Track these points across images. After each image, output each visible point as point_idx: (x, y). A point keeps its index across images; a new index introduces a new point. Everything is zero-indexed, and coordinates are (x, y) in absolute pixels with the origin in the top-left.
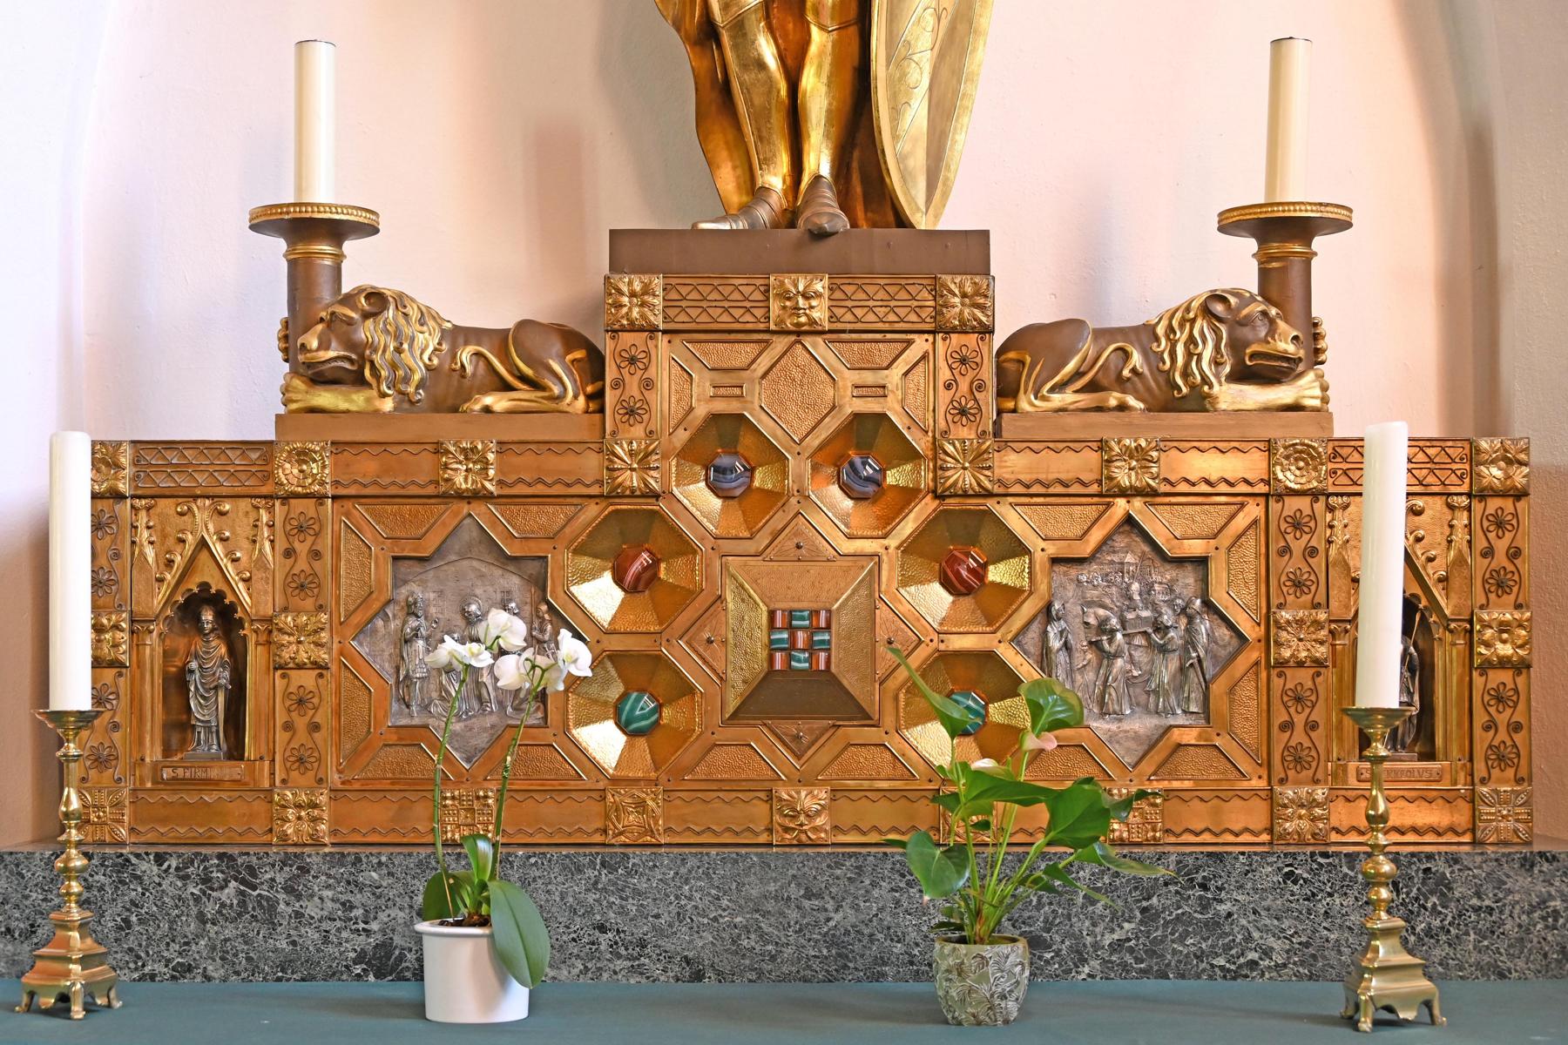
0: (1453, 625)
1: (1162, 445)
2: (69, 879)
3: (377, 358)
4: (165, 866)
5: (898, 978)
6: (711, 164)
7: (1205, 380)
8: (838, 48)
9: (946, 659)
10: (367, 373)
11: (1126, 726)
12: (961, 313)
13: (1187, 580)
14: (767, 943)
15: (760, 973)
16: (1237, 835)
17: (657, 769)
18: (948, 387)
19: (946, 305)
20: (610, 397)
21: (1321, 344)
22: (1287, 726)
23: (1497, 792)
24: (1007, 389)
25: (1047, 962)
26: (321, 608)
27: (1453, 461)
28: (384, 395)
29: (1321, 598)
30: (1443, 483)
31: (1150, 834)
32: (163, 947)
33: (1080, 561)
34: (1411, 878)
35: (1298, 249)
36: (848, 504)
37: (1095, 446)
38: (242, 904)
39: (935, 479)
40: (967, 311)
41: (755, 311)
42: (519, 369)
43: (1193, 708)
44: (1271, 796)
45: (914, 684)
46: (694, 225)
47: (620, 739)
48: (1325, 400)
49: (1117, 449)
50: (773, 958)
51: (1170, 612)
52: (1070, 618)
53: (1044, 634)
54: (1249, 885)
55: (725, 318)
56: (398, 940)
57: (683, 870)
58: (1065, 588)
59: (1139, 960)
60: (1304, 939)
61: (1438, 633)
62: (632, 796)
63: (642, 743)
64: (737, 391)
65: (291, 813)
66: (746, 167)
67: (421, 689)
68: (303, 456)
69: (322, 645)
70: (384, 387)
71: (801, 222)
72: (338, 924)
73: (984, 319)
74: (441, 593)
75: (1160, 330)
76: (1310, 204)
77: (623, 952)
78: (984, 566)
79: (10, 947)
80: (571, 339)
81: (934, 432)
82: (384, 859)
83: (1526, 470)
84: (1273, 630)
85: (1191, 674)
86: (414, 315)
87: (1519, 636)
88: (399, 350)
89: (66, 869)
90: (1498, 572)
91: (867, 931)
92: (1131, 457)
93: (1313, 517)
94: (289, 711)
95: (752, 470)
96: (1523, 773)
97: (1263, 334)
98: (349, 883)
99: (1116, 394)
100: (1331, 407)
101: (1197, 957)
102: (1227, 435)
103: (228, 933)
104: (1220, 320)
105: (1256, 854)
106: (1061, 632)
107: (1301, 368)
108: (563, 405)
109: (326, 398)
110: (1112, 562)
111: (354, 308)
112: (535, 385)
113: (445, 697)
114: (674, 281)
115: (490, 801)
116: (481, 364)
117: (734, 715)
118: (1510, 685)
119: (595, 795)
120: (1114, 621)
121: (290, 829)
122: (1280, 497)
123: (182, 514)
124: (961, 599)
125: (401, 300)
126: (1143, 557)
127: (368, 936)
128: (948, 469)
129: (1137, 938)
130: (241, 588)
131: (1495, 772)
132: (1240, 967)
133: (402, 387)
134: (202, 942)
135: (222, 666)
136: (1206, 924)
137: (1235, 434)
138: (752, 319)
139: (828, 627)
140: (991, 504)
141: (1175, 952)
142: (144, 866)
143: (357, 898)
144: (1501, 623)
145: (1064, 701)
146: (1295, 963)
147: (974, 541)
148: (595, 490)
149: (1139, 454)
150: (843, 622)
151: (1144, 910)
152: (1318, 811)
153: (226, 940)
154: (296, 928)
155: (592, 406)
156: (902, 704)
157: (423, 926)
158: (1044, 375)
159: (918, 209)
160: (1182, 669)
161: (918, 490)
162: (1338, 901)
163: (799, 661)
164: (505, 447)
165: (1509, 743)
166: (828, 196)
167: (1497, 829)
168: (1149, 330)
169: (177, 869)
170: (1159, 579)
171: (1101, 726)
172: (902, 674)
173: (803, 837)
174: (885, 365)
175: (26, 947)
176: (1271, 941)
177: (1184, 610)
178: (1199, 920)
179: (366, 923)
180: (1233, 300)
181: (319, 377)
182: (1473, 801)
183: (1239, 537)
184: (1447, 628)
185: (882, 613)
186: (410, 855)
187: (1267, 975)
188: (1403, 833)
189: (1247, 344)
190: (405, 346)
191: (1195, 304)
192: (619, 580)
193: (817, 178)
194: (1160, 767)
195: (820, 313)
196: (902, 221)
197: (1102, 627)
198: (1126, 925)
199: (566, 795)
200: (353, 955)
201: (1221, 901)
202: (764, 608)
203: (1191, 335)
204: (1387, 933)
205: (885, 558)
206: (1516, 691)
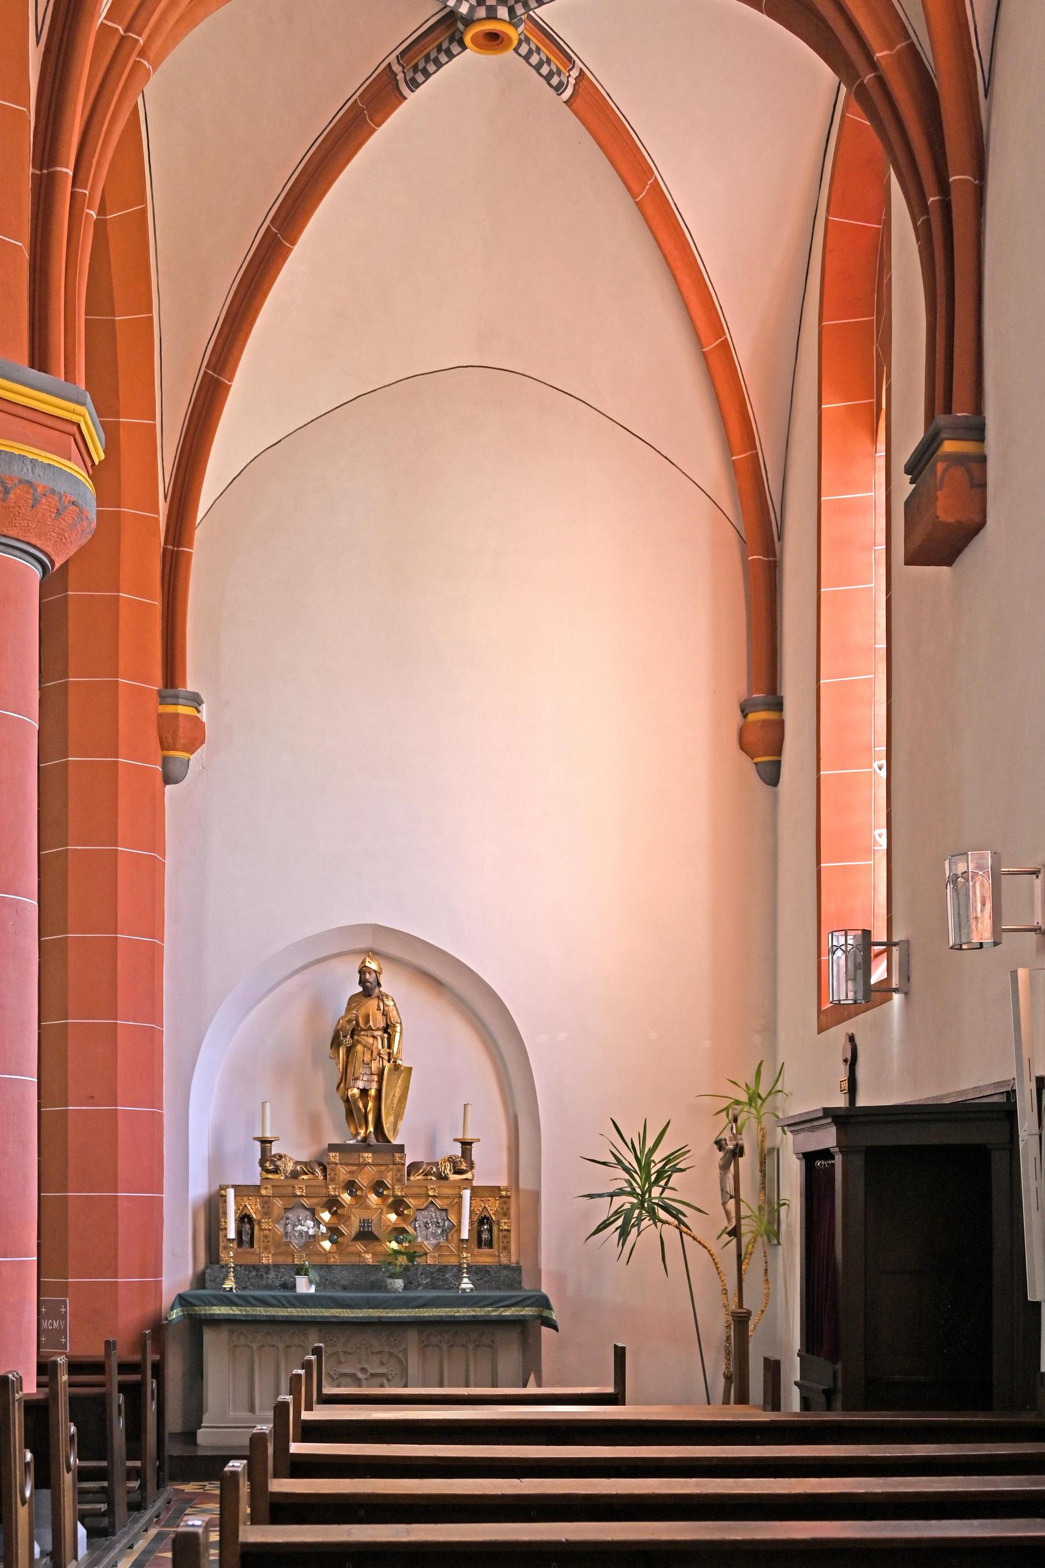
3: (281, 1168)
8: (374, 1106)
11: (431, 1242)
13: (444, 1213)
20: (328, 1177)
28: (282, 1176)
65: (264, 1259)
75: (440, 1164)
80: (320, 1164)
88: (285, 1167)
109: (270, 1176)
112: (313, 1174)
121: (264, 1262)
150: (374, 1221)
161: (390, 1195)
166: (372, 1136)
180: (454, 1158)
181: (268, 1171)
192: (330, 1212)
195: (370, 1161)
197: (427, 1223)
204: (465, 1277)
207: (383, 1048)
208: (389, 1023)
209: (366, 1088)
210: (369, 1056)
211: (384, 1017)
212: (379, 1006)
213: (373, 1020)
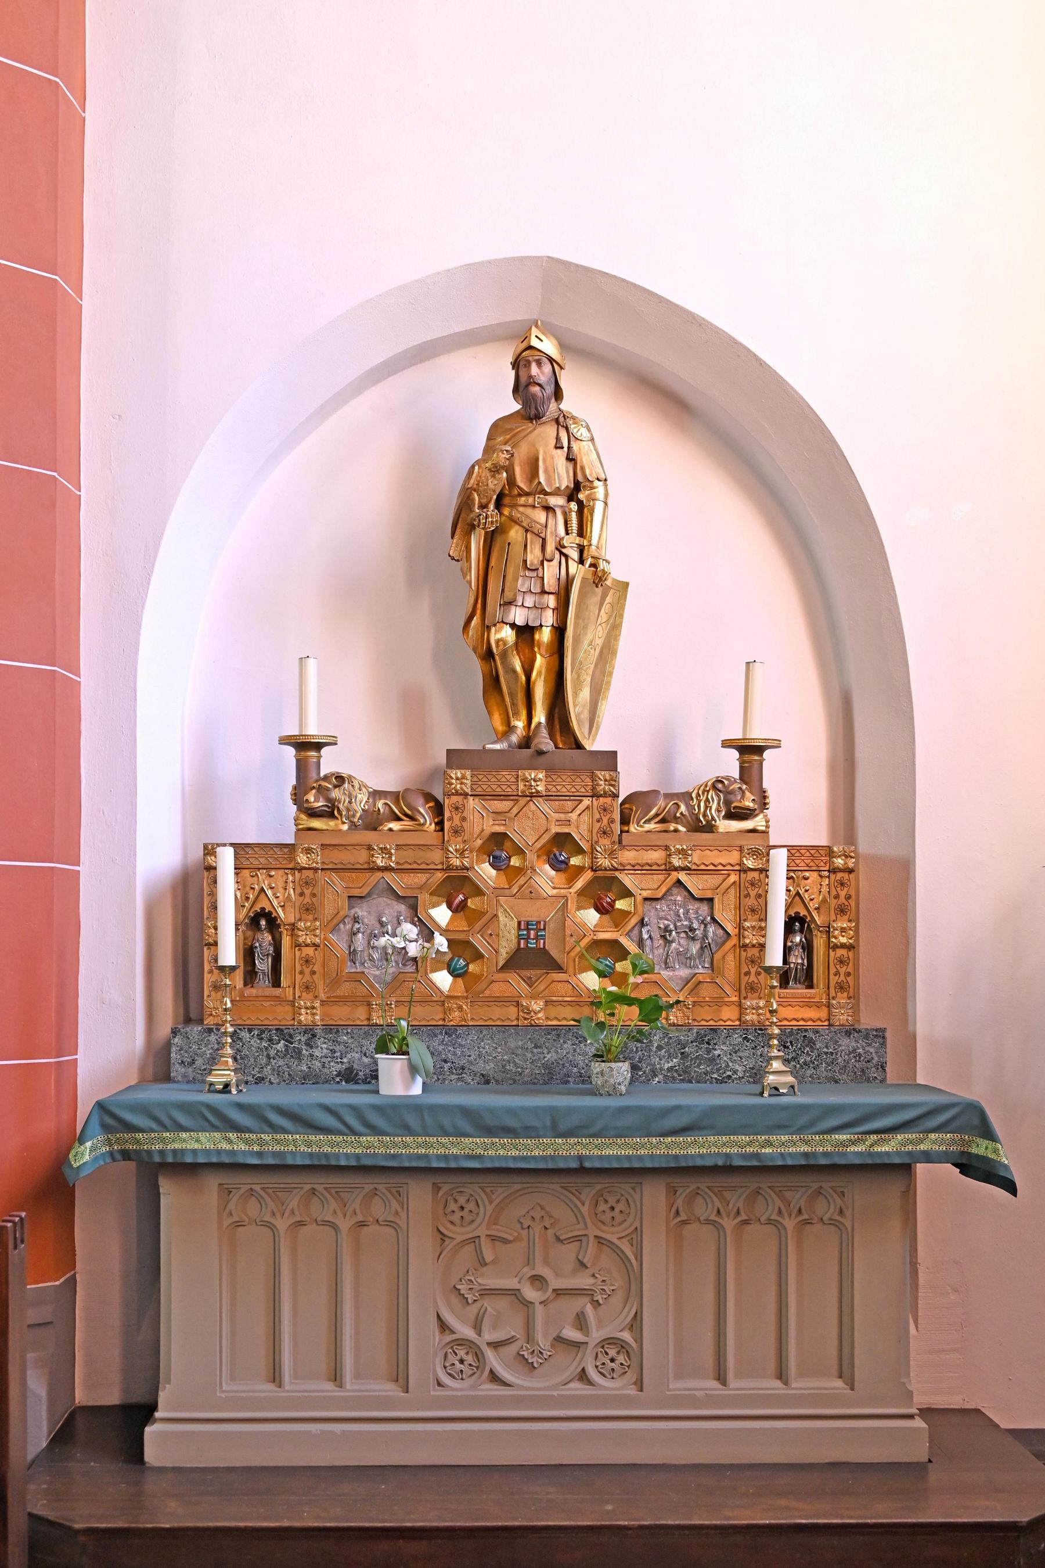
0: (821, 929)
1: (693, 848)
2: (227, 1036)
3: (341, 806)
4: (252, 1034)
5: (575, 1082)
6: (490, 714)
7: (713, 819)
9: (597, 944)
10: (336, 813)
11: (676, 973)
12: (604, 788)
13: (704, 909)
14: (518, 1067)
15: (515, 1081)
16: (725, 1022)
17: (467, 992)
18: (598, 821)
19: (598, 785)
20: (447, 825)
21: (767, 801)
22: (748, 973)
23: (839, 1003)
24: (625, 821)
25: (640, 1076)
26: (316, 919)
27: (822, 856)
28: (344, 823)
29: (763, 917)
30: (817, 866)
31: (687, 1021)
32: (251, 1069)
33: (657, 899)
34: (798, 1040)
35: (756, 758)
36: (553, 873)
37: (663, 848)
38: (286, 1050)
39: (592, 862)
40: (607, 787)
41: (512, 786)
42: (404, 810)
43: (706, 966)
44: (740, 1005)
45: (583, 954)
46: (484, 747)
47: (450, 978)
48: (767, 827)
49: (673, 850)
50: (520, 1074)
51: (696, 922)
52: (652, 925)
53: (641, 932)
54: (728, 1043)
55: (499, 789)
56: (355, 1066)
57: (481, 1036)
58: (650, 911)
59: (680, 1075)
60: (751, 1066)
61: (815, 932)
62: (456, 1004)
63: (460, 980)
64: (504, 822)
66: (505, 714)
67: (360, 956)
68: (308, 851)
69: (317, 936)
70: (344, 819)
71: (533, 745)
72: (329, 1059)
73: (614, 791)
74: (369, 912)
75: (694, 795)
76: (758, 739)
77: (454, 1071)
78: (614, 901)
79: (183, 1070)
81: (592, 841)
82: (349, 1031)
83: (854, 860)
84: (742, 931)
85: (706, 951)
86: (357, 785)
87: (849, 934)
88: (350, 802)
89: (225, 1032)
90: (841, 906)
91: (561, 1062)
92: (680, 854)
93: (760, 880)
94: (302, 965)
95: (510, 858)
96: (851, 994)
97: (739, 798)
98: (334, 1041)
99: (673, 825)
100: (771, 830)
101: (705, 1074)
102: (721, 843)
103: (280, 1063)
104: (720, 791)
105: (731, 1029)
106: (648, 931)
107: (757, 812)
108: (425, 828)
109: (316, 823)
110: (671, 900)
111: (330, 783)
112: (412, 818)
113: (372, 960)
114: (475, 773)
115: (393, 1006)
116: (387, 808)
117: (502, 968)
118: (846, 956)
119: (440, 1003)
120: (672, 927)
121: (302, 1018)
122: (745, 871)
123: (252, 876)
124: (604, 916)
125: (351, 779)
126: (685, 898)
127: (342, 1065)
128: (598, 858)
129: (679, 1066)
130: (280, 910)
131: (839, 994)
132: (723, 1078)
133: (352, 819)
134: (269, 1067)
135: (270, 945)
136: (709, 1059)
137: (725, 843)
138: (511, 790)
139: (544, 929)
140: (617, 874)
141: (695, 1072)
142: (243, 1034)
143: (337, 1048)
144: (842, 928)
145: (647, 963)
146: (747, 1077)
147: (609, 890)
148: (440, 867)
149: (683, 852)
150: (551, 926)
151: (682, 1053)
152: (761, 1011)
153: (279, 1066)
154: (310, 1061)
155: (438, 828)
156: (577, 963)
157: (377, 1056)
158: (642, 815)
159: (585, 737)
160: (702, 948)
162: (766, 1050)
163: (531, 944)
164: (399, 847)
165: (845, 981)
166: (544, 732)
167: (839, 1019)
168: (688, 795)
169: (258, 1035)
170: (692, 907)
171: (665, 974)
172: (577, 949)
173: (533, 1022)
174: (570, 811)
175: (190, 1070)
176: (737, 1067)
177: (703, 922)
178: (706, 1058)
179: (341, 1059)
180: (726, 782)
181: (313, 814)
182: (829, 1007)
183: (727, 889)
184: (818, 930)
185: (568, 923)
186: (361, 1029)
187: (735, 1082)
188: (798, 1021)
189: (732, 802)
190: (353, 800)
191: (710, 783)
192: (449, 907)
193: (540, 723)
194: (692, 991)
196: (579, 746)
197: (666, 929)
198: (674, 1060)
199: (427, 1003)
200: (335, 1073)
201: (715, 1050)
202: (516, 920)
203: (707, 798)
204: (776, 1058)
205: (569, 898)
206: (848, 958)
207: (567, 533)
208: (580, 478)
210: (537, 551)
212: (558, 438)
213: (546, 471)
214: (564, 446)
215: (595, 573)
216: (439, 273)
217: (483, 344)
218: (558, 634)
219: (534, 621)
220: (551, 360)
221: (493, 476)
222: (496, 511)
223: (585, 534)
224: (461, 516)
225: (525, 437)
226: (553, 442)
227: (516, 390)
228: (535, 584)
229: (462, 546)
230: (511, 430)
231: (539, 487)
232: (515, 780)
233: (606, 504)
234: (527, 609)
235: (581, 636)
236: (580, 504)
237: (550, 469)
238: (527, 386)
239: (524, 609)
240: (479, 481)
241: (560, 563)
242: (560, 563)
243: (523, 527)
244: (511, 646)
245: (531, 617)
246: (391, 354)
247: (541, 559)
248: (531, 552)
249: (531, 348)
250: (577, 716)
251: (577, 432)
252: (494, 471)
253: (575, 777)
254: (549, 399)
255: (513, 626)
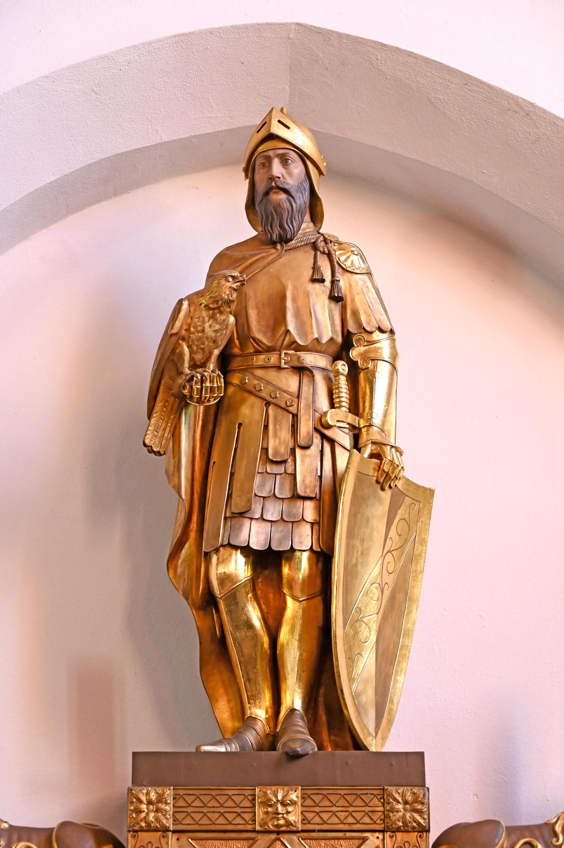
6: (212, 699)
12: (404, 816)
19: (392, 810)
40: (408, 815)
46: (198, 748)
55: (221, 821)
71: (279, 746)
73: (422, 821)
114: (181, 792)
138: (241, 822)
159: (369, 734)
166: (300, 724)
196: (358, 745)
207: (332, 406)
208: (351, 327)
209: (274, 547)
210: (285, 434)
211: (336, 309)
212: (315, 268)
213: (297, 315)
214: (325, 277)
215: (379, 468)
216: (135, 47)
217: (207, 169)
218: (320, 565)
219: (280, 542)
220: (303, 156)
221: (213, 317)
222: (218, 372)
223: (361, 411)
224: (163, 382)
225: (264, 268)
226: (308, 273)
227: (250, 205)
228: (282, 485)
229: (164, 430)
230: (244, 259)
231: (287, 338)
232: (249, 805)
233: (394, 367)
234: (269, 524)
235: (359, 566)
236: (353, 366)
237: (304, 311)
238: (267, 193)
239: (264, 524)
240: (189, 325)
241: (322, 452)
242: (322, 452)
243: (262, 398)
244: (244, 585)
245: (276, 536)
246: (68, 171)
247: (291, 445)
248: (275, 435)
249: (271, 137)
250: (355, 697)
251: (346, 260)
252: (214, 309)
253: (353, 797)
254: (301, 213)
255: (246, 550)
